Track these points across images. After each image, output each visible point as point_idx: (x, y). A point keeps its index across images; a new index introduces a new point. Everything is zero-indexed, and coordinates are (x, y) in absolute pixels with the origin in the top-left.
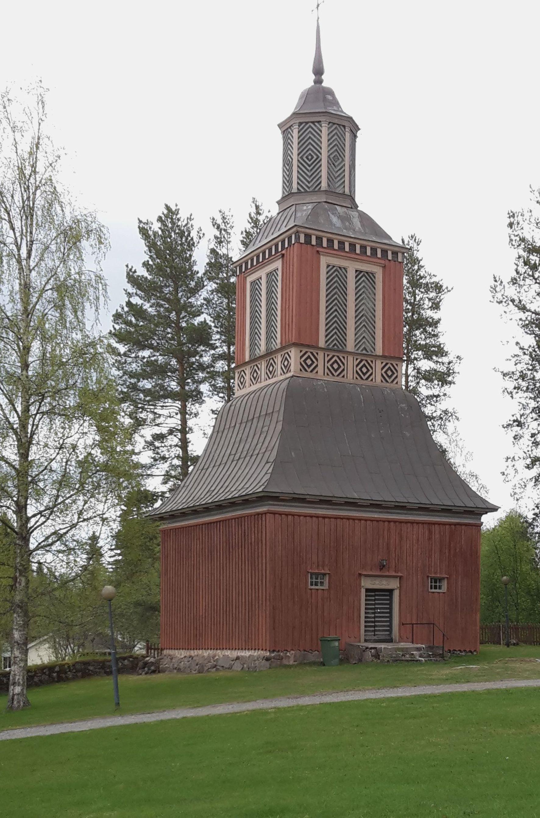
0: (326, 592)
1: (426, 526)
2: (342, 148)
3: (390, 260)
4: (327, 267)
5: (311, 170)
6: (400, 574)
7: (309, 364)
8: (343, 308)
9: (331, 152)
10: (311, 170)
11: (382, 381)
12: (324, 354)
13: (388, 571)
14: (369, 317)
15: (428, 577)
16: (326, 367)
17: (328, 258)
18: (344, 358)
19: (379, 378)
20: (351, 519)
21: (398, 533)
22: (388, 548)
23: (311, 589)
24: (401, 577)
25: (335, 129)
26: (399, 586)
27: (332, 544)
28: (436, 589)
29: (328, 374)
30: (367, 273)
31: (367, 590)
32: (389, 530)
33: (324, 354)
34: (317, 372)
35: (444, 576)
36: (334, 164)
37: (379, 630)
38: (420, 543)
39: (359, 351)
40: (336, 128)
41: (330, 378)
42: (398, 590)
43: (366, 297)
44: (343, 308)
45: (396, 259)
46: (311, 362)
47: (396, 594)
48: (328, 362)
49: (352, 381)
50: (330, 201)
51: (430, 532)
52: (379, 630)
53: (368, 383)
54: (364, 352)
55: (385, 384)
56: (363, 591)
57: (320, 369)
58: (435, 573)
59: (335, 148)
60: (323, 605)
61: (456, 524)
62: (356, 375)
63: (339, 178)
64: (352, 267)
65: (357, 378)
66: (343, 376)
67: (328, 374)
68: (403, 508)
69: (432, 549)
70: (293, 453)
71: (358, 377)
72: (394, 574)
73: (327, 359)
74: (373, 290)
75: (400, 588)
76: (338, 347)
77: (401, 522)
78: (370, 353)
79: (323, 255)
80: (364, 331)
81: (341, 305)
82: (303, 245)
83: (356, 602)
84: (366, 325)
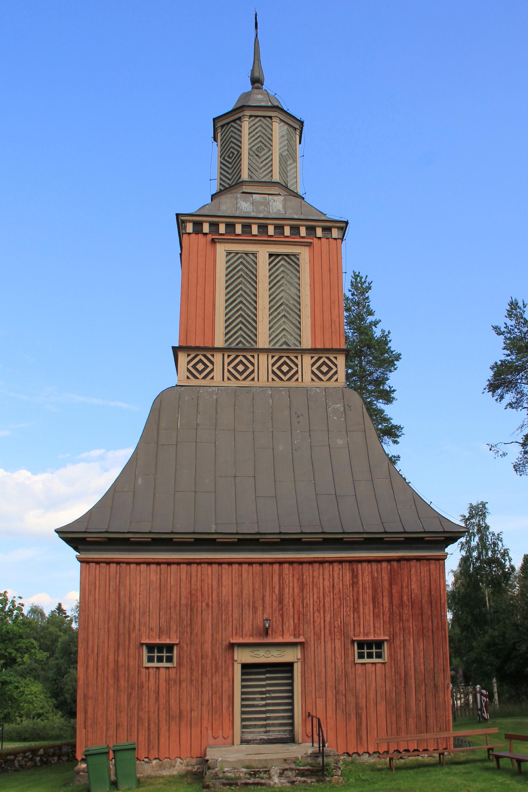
0: (173, 672)
1: (346, 566)
2: (269, 138)
3: (320, 238)
4: (227, 256)
5: (232, 167)
6: (301, 639)
7: (197, 367)
8: (252, 299)
9: (252, 145)
10: (232, 167)
11: (312, 380)
12: (223, 355)
13: (283, 636)
14: (290, 305)
15: (353, 642)
16: (226, 371)
17: (226, 245)
18: (253, 357)
19: (308, 376)
20: (215, 563)
21: (298, 579)
22: (281, 601)
23: (147, 668)
24: (302, 644)
25: (258, 121)
26: (299, 657)
27: (183, 601)
28: (372, 657)
29: (229, 379)
30: (287, 255)
31: (245, 666)
32: (280, 575)
33: (223, 355)
34: (212, 378)
35: (382, 638)
36: (257, 155)
37: (273, 725)
38: (336, 591)
39: (277, 347)
40: (260, 120)
41: (233, 383)
42: (299, 664)
43: (286, 282)
44: (252, 299)
45: (329, 236)
46: (200, 364)
47: (297, 669)
48: (229, 364)
49: (266, 384)
50: (248, 191)
51: (354, 576)
52: (273, 725)
53: (292, 384)
54: (284, 347)
55: (318, 383)
56: (238, 669)
57: (217, 374)
58: (367, 634)
59: (258, 140)
60: (168, 691)
61: (399, 560)
62: (271, 376)
63: (264, 169)
64: (263, 253)
65: (273, 380)
66: (253, 379)
67: (229, 379)
68: (298, 542)
69: (358, 600)
70: (140, 480)
71: (275, 378)
72: (292, 640)
73: (227, 361)
74: (298, 274)
75: (304, 660)
76: (245, 345)
77: (301, 563)
78: (292, 347)
79: (220, 242)
80: (284, 322)
81: (249, 296)
82: (191, 235)
83: (226, 684)
84: (287, 315)
